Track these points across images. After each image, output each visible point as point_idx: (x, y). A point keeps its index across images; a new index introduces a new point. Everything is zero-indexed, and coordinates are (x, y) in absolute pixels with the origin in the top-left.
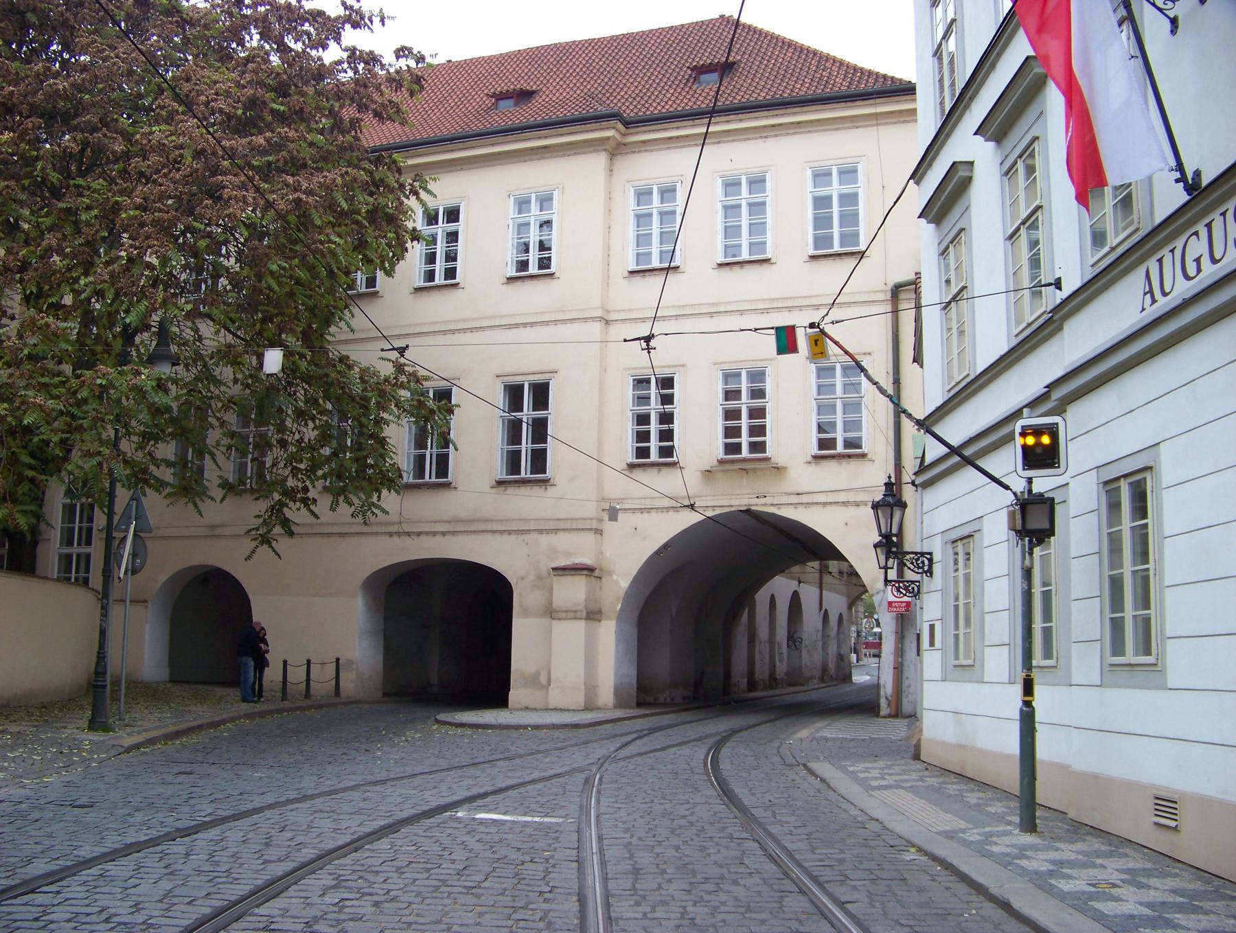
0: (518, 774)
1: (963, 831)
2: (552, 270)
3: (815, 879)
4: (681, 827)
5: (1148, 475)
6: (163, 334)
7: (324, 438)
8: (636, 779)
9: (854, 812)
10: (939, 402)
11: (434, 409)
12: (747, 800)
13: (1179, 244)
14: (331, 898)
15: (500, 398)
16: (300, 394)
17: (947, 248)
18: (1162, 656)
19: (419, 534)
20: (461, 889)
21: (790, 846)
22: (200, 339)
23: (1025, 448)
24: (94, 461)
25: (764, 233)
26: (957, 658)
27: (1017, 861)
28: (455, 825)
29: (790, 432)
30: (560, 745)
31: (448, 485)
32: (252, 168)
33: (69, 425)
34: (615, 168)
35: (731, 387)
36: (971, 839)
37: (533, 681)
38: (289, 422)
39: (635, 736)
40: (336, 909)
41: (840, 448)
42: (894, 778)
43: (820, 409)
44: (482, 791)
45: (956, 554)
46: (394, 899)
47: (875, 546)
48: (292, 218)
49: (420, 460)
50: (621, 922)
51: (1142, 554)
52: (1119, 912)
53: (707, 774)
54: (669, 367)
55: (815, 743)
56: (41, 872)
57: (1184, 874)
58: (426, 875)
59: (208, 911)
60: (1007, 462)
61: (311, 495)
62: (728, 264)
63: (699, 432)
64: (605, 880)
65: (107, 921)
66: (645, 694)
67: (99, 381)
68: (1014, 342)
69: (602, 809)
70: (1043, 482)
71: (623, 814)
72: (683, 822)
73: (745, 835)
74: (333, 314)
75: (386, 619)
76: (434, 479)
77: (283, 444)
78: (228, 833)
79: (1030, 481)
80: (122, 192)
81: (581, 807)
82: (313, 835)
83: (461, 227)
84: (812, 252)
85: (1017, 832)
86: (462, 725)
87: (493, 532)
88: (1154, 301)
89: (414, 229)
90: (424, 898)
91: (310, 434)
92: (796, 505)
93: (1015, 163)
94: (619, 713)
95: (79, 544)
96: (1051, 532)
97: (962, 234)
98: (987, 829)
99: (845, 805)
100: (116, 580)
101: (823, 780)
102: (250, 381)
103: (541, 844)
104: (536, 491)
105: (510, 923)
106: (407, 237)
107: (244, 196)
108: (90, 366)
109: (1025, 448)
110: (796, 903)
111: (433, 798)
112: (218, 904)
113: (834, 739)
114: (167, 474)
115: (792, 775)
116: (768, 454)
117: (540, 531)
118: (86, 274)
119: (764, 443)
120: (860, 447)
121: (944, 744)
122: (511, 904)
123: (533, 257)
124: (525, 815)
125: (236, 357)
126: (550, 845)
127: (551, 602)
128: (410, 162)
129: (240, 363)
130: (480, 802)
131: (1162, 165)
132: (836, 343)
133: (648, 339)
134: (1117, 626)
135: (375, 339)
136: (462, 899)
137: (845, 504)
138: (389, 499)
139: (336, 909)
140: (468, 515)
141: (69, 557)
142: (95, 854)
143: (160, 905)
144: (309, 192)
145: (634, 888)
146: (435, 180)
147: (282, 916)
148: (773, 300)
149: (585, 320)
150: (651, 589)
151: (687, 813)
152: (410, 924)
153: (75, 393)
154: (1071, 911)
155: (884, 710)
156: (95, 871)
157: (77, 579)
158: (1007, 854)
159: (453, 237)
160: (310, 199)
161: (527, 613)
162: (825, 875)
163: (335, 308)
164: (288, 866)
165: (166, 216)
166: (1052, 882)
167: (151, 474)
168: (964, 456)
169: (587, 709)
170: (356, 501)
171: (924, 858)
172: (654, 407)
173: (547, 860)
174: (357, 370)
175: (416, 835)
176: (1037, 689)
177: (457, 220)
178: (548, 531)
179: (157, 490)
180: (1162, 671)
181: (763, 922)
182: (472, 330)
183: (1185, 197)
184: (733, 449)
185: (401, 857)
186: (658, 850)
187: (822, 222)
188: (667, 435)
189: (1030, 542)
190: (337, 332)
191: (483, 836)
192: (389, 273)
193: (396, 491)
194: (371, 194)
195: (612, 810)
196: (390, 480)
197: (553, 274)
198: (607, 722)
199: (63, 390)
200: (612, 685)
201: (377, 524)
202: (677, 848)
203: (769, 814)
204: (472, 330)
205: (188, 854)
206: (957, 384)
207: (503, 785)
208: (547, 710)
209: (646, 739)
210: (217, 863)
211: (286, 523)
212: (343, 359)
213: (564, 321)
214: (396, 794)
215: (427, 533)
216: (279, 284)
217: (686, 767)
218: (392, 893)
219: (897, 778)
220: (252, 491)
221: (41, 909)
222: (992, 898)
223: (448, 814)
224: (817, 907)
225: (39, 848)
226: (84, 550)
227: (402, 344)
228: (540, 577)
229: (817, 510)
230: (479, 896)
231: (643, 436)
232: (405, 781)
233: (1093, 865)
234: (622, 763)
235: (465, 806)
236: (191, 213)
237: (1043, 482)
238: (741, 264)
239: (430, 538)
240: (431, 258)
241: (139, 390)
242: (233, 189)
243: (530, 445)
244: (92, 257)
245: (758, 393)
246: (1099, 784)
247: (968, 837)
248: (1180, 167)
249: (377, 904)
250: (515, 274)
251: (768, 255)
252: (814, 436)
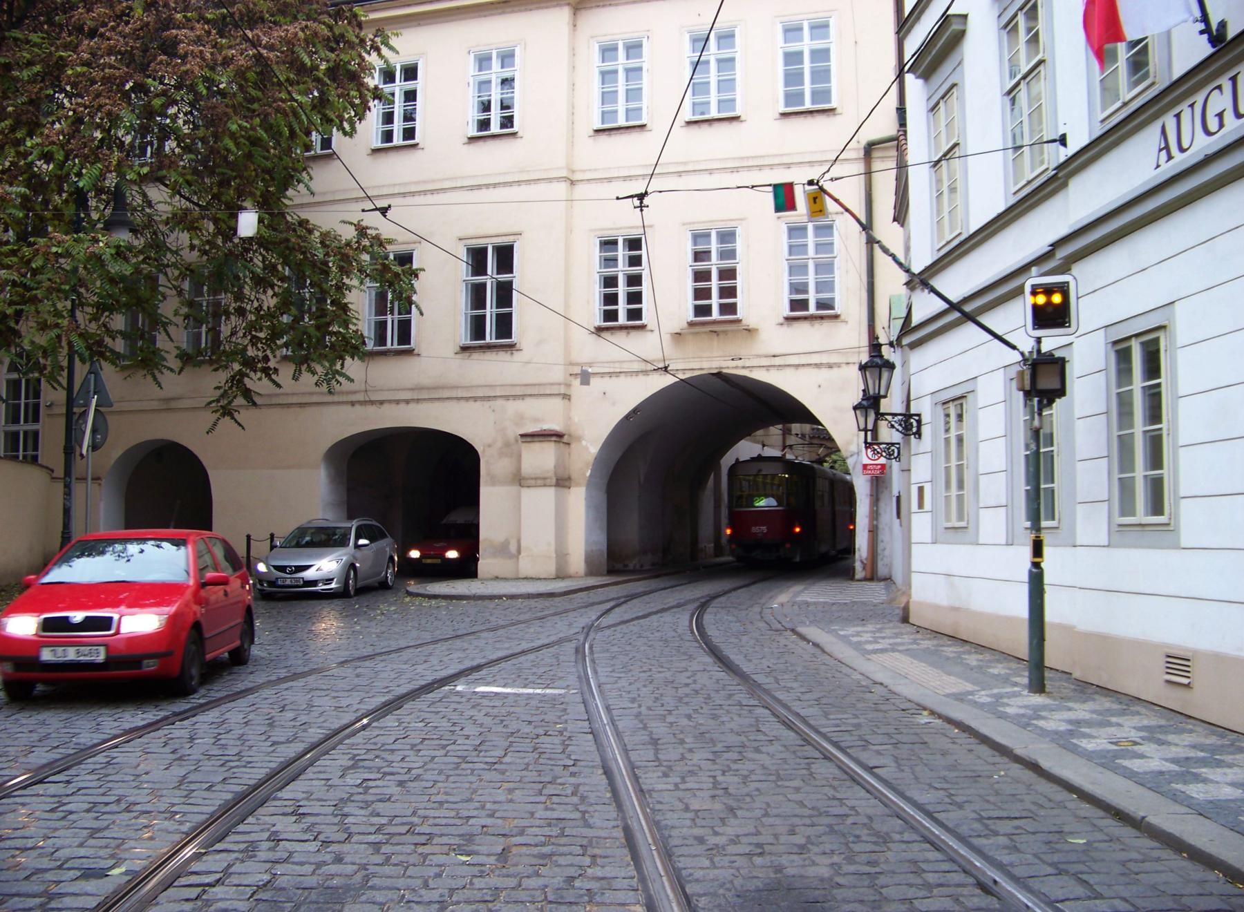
0: (507, 645)
1: (972, 693)
2: (515, 129)
3: (836, 744)
4: (687, 695)
5: (1161, 334)
6: (117, 197)
7: (284, 306)
8: (628, 648)
9: (856, 676)
10: (929, 262)
11: (396, 275)
12: (746, 667)
13: (1199, 98)
14: (353, 779)
16: (258, 261)
17: (937, 104)
18: (1175, 515)
19: (382, 402)
20: (483, 766)
21: (803, 713)
22: (150, 205)
23: (1035, 308)
24: (53, 333)
25: (733, 90)
26: (948, 519)
27: (1035, 722)
28: (457, 699)
29: (762, 294)
30: (539, 614)
32: (208, 22)
33: (23, 296)
34: (579, 23)
35: (700, 248)
36: (982, 700)
37: (501, 550)
38: (247, 290)
39: (612, 604)
40: (361, 790)
41: (812, 309)
42: (888, 641)
43: (793, 269)
44: (475, 663)
45: (948, 416)
46: (417, 778)
47: (855, 408)
48: (251, 75)
49: (381, 326)
50: (654, 795)
51: (1154, 413)
52: (1148, 769)
53: (697, 641)
55: (796, 607)
56: (44, 761)
57: (1199, 729)
58: (442, 752)
59: (229, 796)
60: (1014, 319)
61: (272, 364)
62: (696, 122)
63: (669, 293)
64: (626, 751)
65: (127, 810)
66: (615, 562)
67: (54, 249)
68: (1013, 200)
69: (603, 680)
70: (1052, 341)
71: (623, 683)
72: (687, 690)
73: (752, 702)
74: (292, 177)
75: (349, 490)
76: (396, 346)
77: (241, 312)
78: (228, 715)
79: (1039, 340)
80: (66, 47)
81: (579, 677)
82: (315, 714)
83: (420, 85)
84: (783, 109)
85: (1025, 692)
86: (435, 597)
87: (458, 399)
88: (1170, 157)
89: (376, 88)
90: (448, 776)
91: (269, 301)
92: (768, 367)
93: (1015, 15)
94: (592, 581)
95: (26, 421)
96: (1061, 392)
97: (954, 90)
98: (995, 691)
99: (845, 670)
100: (78, 458)
101: (816, 645)
102: (207, 247)
103: (550, 717)
104: (503, 356)
105: (543, 799)
106: (369, 95)
107: (201, 52)
108: (41, 232)
109: (1035, 308)
110: (824, 769)
111: (428, 673)
112: (238, 789)
113: (815, 603)
114: (119, 345)
115: (783, 641)
116: (739, 316)
117: (507, 397)
118: (31, 135)
119: (640, 310)
120: (832, 308)
121: (937, 608)
122: (538, 779)
123: (495, 115)
124: (525, 686)
125: (192, 222)
126: (560, 717)
127: (519, 469)
128: (373, 16)
129: (197, 228)
130: (475, 675)
131: (1186, 16)
132: (836, 200)
133: (641, 197)
134: (1126, 488)
135: (357, 200)
136: (487, 776)
137: (818, 366)
138: (352, 366)
139: (361, 790)
140: (433, 382)
141: (17, 434)
142: (95, 741)
143: (177, 792)
144: (271, 48)
145: (658, 759)
146: (397, 35)
147: (307, 799)
148: (742, 158)
149: (550, 180)
150: (619, 454)
151: (689, 681)
152: (441, 803)
153: (29, 262)
154: (1100, 769)
155: (860, 573)
156: (101, 758)
157: (25, 457)
158: (1023, 715)
159: (411, 96)
160: (271, 55)
161: (494, 481)
162: (847, 740)
163: (295, 170)
164: (299, 747)
165: (117, 73)
166: (1074, 741)
167: (106, 347)
168: (963, 312)
169: (560, 576)
170: (319, 369)
171: (939, 721)
172: (622, 269)
173: (561, 733)
174: (317, 234)
175: (420, 711)
176: (1047, 550)
177: (415, 78)
178: (515, 397)
179: (113, 363)
180: (1176, 531)
181: (797, 790)
182: (432, 192)
183: (1208, 50)
184: (702, 311)
185: (413, 734)
186: (670, 719)
187: (792, 78)
188: (635, 298)
189: (1040, 402)
190: (295, 195)
191: (489, 710)
192: (350, 134)
193: (361, 359)
194: (332, 50)
195: (612, 680)
196: (352, 346)
197: (416, 145)
198: (581, 590)
199: (15, 259)
200: (583, 553)
201: (342, 393)
202: (689, 717)
203: (771, 680)
204: (432, 192)
205: (192, 739)
206: (948, 243)
207: (494, 657)
208: (518, 579)
209: (624, 607)
210: (224, 746)
211: (247, 393)
212: (303, 223)
213: (528, 182)
214: (388, 669)
215: (390, 401)
216: (237, 145)
217: (674, 634)
218: (413, 772)
219: (892, 641)
220: (211, 362)
221: (56, 799)
222: (1018, 759)
223: (447, 688)
224: (846, 773)
225: (35, 736)
226: (31, 427)
227: (382, 203)
228: (507, 445)
229: (789, 372)
230: (503, 772)
231: (611, 299)
232: (393, 655)
233: (1110, 724)
234: (607, 632)
235: (463, 680)
236: (144, 68)
237: (1052, 341)
238: (710, 121)
239: (393, 406)
240: (388, 118)
241: (98, 259)
242: (189, 45)
243: (494, 310)
244: (37, 117)
245: (729, 254)
246: (1105, 644)
247: (976, 698)
248: (1205, 18)
249: (401, 784)
250: (476, 134)
251: (833, 105)
252: (785, 297)
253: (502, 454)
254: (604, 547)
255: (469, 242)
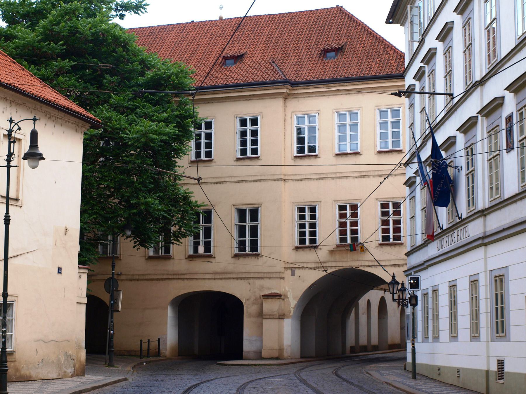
15: (235, 217)
41: (391, 240)
54: (314, 202)
76: (163, 255)
140: (221, 271)
213: (265, 180)
228: (256, 299)
254: (177, 345)
255: (237, 207)
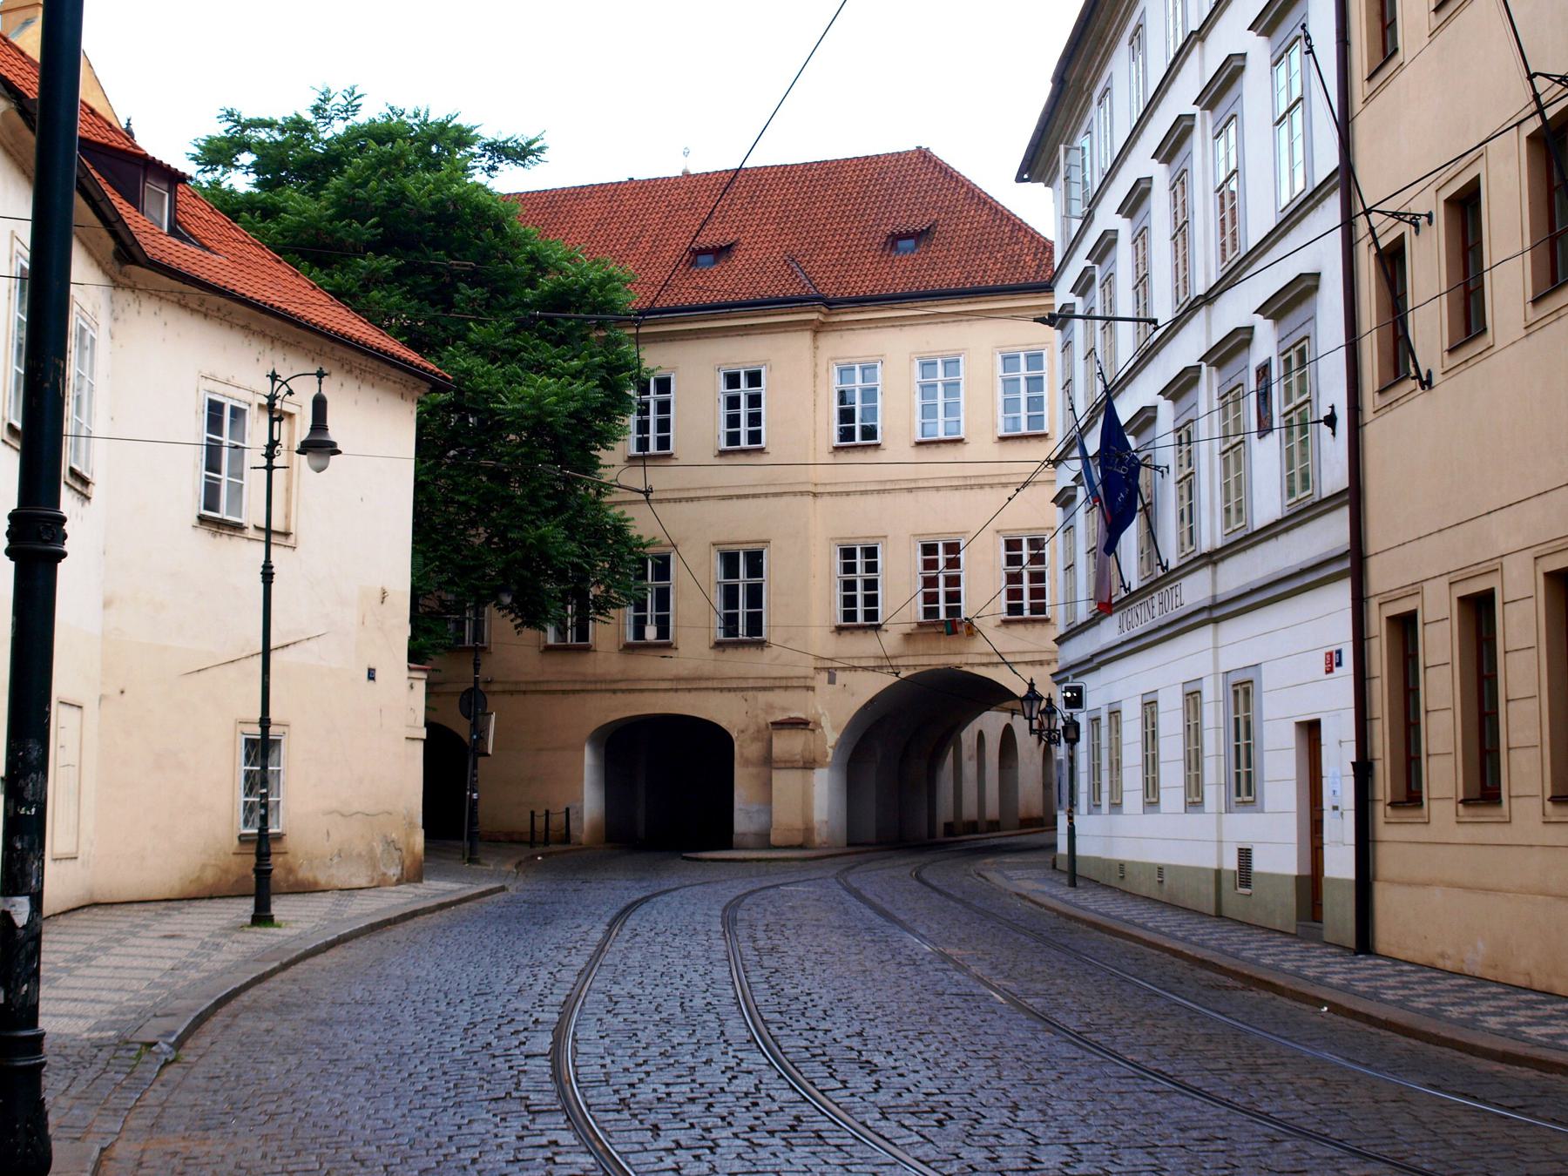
31: (669, 646)
41: (1027, 614)
172: (860, 573)
178: (764, 689)
240: (643, 427)
253: (754, 739)
